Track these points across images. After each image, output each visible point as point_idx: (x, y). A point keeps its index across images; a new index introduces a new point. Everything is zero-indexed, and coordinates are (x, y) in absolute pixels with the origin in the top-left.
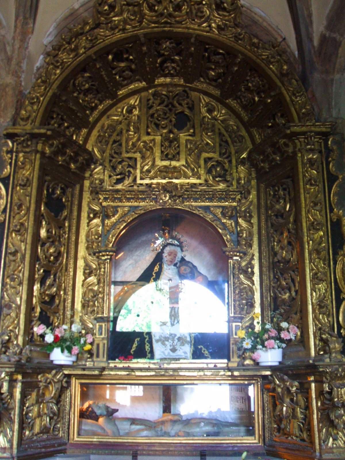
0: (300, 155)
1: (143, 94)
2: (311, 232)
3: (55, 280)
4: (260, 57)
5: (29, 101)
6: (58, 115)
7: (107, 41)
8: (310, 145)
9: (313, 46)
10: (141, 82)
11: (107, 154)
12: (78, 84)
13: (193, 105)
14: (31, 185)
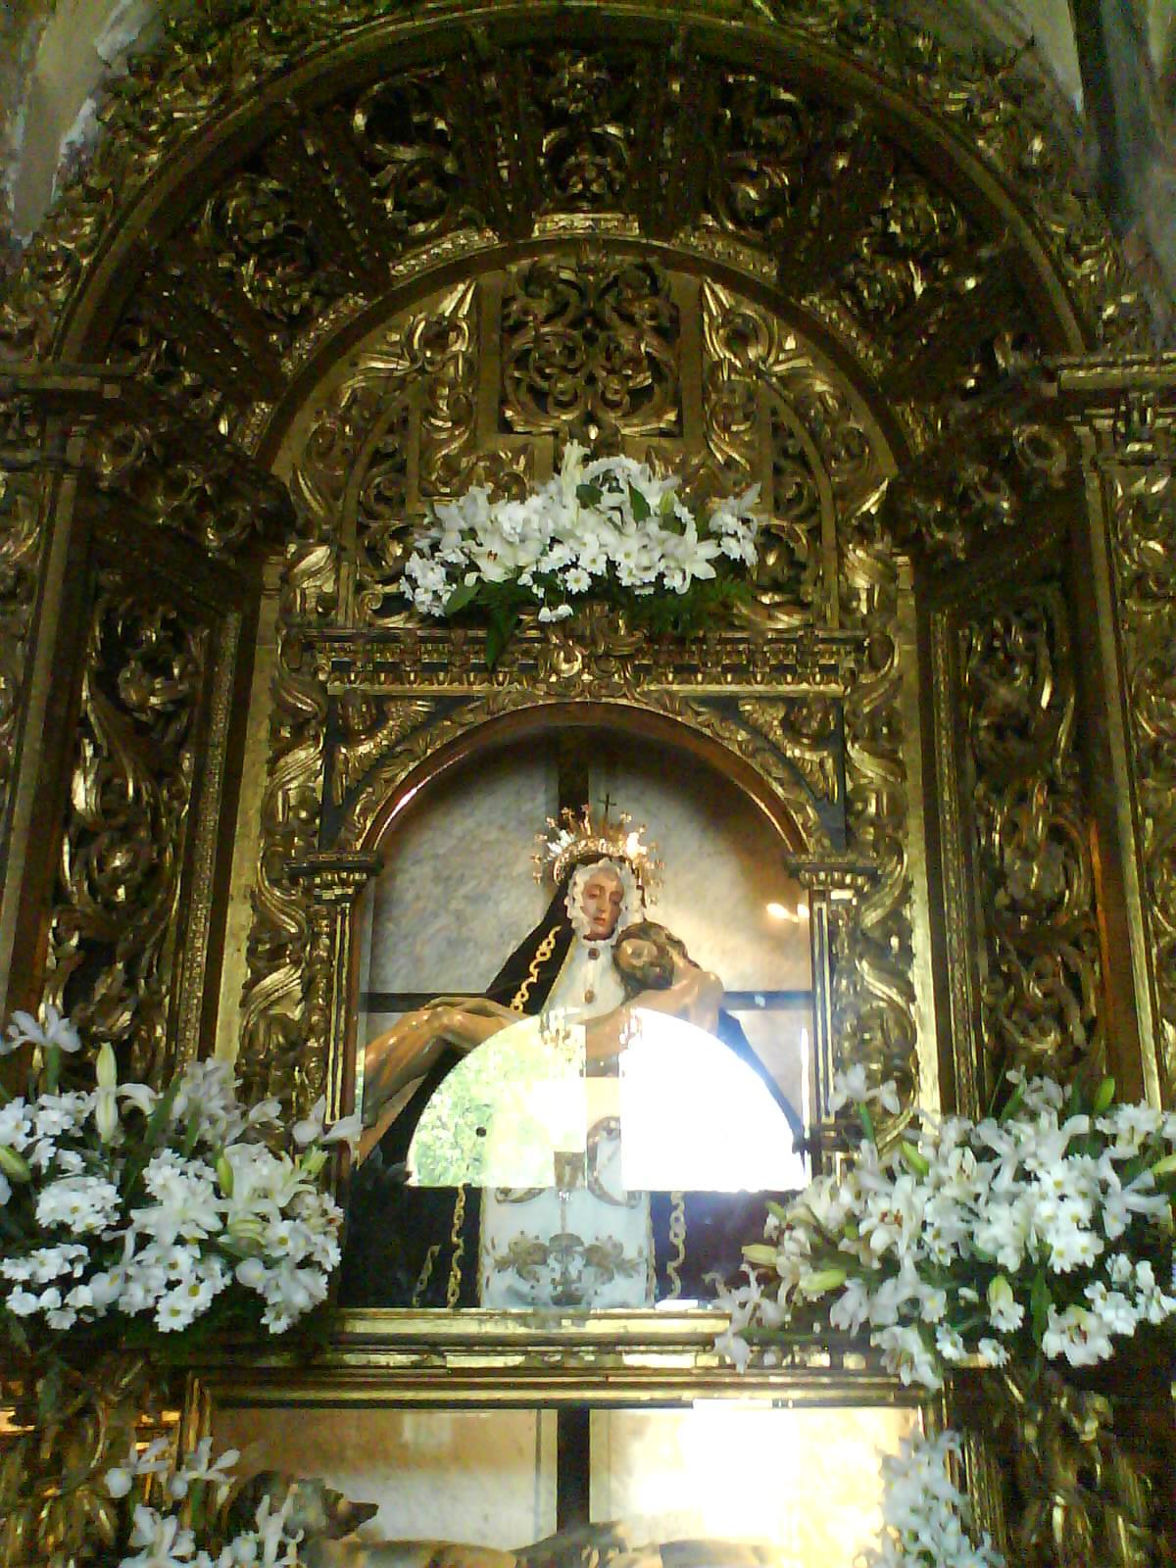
0: (1095, 484)
1: (488, 279)
2: (1150, 782)
3: (131, 982)
4: (936, 110)
5: (32, 271)
6: (156, 337)
7: (342, 48)
8: (1139, 440)
9: (1149, 67)
10: (480, 230)
11: (347, 505)
12: (235, 218)
13: (675, 321)
14: (34, 595)
